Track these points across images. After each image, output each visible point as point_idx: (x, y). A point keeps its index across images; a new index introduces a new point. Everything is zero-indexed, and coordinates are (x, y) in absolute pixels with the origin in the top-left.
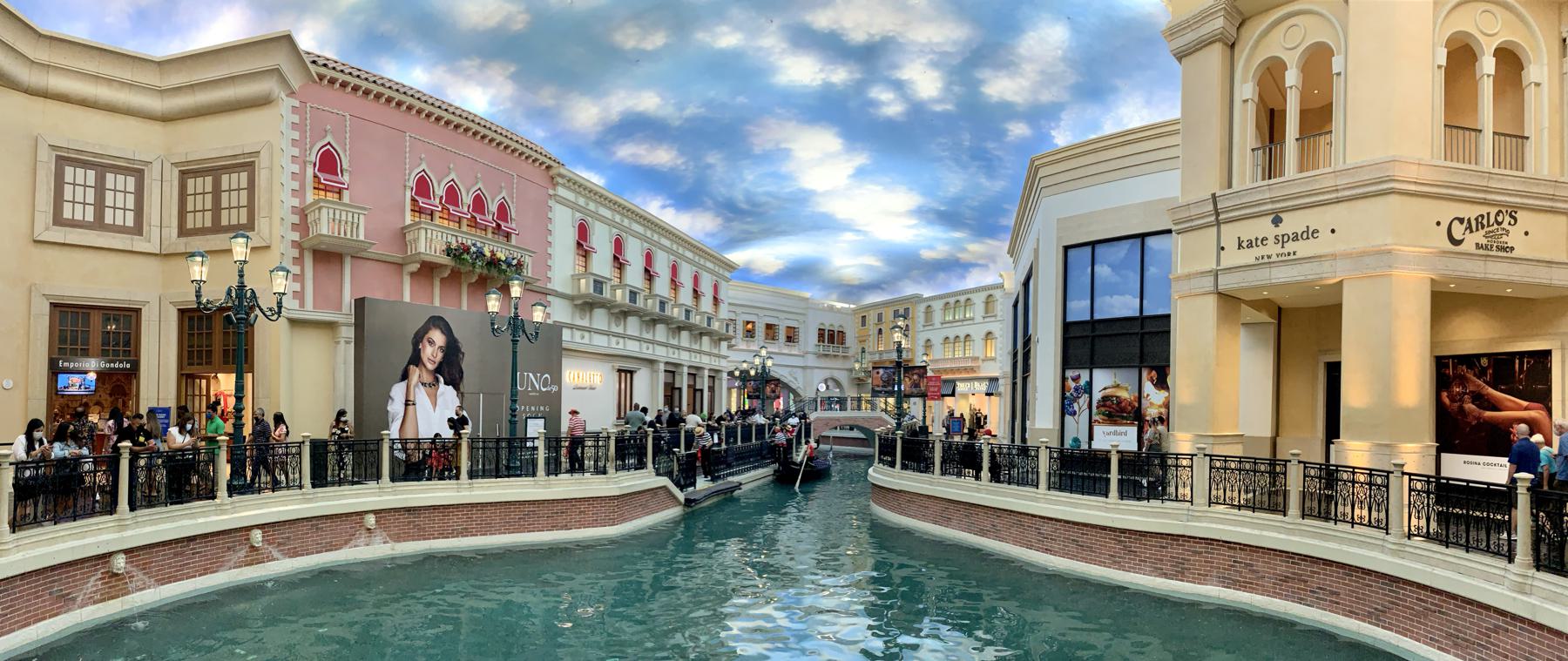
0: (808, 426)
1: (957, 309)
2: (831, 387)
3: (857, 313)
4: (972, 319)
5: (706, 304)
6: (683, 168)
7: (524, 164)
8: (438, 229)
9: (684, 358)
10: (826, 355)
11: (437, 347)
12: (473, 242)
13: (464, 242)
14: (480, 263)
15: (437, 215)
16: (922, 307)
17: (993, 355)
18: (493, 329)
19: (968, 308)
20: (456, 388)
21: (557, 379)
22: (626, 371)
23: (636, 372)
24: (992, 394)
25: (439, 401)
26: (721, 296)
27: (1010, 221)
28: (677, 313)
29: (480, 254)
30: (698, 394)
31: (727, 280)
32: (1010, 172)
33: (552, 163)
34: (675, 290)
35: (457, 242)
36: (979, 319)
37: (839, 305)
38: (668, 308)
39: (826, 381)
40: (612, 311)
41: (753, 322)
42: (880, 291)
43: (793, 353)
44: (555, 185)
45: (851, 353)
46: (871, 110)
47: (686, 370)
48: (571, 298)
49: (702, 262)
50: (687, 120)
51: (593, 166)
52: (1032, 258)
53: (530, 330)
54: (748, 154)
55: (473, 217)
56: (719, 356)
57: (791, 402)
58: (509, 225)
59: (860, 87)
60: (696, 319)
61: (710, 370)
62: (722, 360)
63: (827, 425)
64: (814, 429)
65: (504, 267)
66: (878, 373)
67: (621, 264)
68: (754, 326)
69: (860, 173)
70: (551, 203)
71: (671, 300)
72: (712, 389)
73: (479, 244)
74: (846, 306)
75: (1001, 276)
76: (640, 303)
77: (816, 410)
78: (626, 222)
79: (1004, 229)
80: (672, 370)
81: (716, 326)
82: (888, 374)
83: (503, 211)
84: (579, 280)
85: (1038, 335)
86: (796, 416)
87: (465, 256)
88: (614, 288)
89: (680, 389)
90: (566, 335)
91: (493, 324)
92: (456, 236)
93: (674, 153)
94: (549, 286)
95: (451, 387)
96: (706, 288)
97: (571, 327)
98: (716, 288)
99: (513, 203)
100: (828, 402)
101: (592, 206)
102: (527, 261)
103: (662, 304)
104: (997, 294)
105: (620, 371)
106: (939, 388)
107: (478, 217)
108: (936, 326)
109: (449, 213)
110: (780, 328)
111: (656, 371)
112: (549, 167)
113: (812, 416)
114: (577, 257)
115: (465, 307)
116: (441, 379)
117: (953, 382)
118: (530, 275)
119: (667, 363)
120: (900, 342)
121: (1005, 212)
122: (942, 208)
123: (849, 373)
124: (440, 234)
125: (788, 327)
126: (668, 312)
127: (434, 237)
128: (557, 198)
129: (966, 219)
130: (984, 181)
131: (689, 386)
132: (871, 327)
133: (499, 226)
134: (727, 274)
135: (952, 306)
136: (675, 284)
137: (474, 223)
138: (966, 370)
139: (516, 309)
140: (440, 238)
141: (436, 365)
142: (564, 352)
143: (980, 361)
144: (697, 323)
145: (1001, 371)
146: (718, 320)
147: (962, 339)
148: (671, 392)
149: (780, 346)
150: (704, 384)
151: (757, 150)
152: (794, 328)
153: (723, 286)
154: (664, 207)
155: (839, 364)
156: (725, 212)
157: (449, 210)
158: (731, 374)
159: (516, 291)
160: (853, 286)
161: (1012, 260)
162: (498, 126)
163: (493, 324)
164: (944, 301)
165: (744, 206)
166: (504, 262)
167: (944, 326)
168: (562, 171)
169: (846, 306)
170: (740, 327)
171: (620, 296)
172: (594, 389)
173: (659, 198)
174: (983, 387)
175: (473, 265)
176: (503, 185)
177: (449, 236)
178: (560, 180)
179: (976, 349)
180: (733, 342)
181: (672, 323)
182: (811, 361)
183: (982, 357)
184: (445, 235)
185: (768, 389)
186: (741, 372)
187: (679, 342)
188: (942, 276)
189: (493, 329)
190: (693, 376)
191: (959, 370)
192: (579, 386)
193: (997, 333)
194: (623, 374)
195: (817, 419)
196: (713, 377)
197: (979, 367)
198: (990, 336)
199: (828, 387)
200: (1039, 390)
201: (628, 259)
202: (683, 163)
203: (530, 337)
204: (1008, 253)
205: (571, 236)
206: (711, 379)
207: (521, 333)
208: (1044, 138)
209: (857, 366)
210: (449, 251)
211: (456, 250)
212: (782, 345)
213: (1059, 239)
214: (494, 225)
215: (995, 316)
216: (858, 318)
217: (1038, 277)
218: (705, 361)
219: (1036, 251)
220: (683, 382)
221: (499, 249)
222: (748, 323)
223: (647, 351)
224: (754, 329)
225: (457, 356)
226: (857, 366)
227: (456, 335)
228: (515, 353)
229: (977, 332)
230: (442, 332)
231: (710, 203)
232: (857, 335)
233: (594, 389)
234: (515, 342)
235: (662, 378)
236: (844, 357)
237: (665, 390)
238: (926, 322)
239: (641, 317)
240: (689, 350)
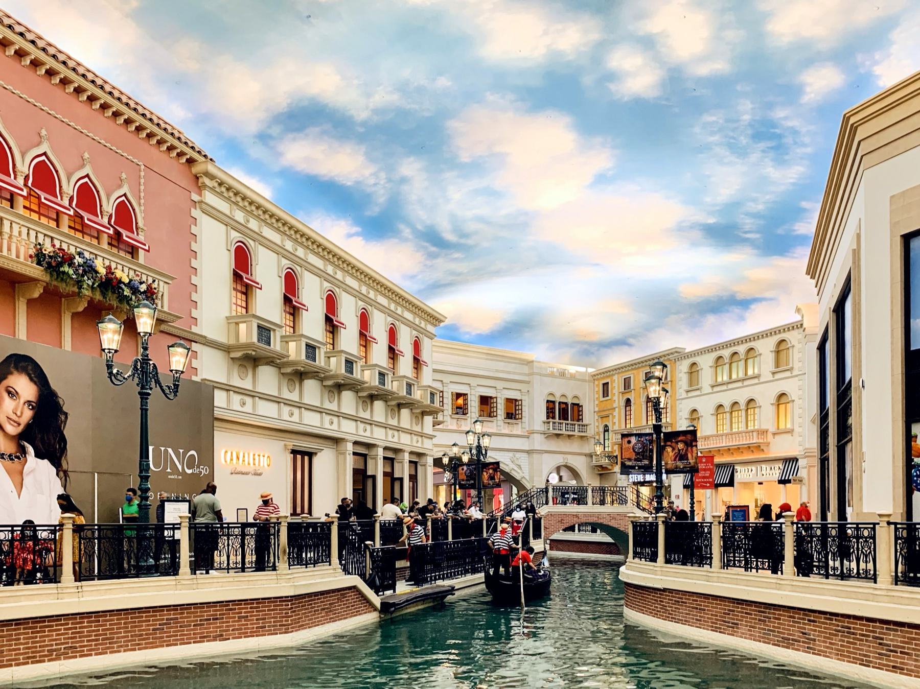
0: (537, 523)
1: (734, 365)
2: (564, 479)
3: (598, 379)
4: (757, 377)
5: (405, 366)
6: (372, 181)
7: (154, 152)
8: (22, 223)
9: (379, 436)
10: (558, 435)
11: (22, 401)
12: (78, 250)
13: (65, 247)
14: (90, 283)
15: (20, 202)
16: (684, 366)
17: (789, 426)
18: (111, 373)
19: (750, 362)
20: (56, 462)
21: (208, 457)
22: (303, 453)
23: (316, 454)
24: (789, 481)
25: (27, 480)
26: (425, 356)
27: (808, 227)
28: (369, 378)
29: (89, 269)
30: (397, 486)
31: (431, 337)
32: (809, 150)
33: (196, 156)
34: (365, 347)
35: (54, 246)
36: (766, 375)
37: (573, 369)
38: (357, 369)
39: (558, 469)
40: (283, 371)
41: (465, 395)
42: (625, 348)
43: (515, 432)
44: (200, 188)
45: (591, 431)
46: (612, 87)
47: (380, 453)
48: (226, 349)
49: (399, 311)
50: (376, 111)
51: (255, 168)
52: (850, 264)
53: (167, 382)
54: (453, 164)
55: (77, 215)
56: (422, 435)
57: (514, 496)
58: (135, 236)
59: (600, 50)
60: (392, 385)
61: (411, 453)
62: (426, 440)
63: (561, 521)
64: (545, 527)
65: (127, 292)
66: (629, 442)
67: (294, 307)
68: (465, 400)
69: (601, 179)
70: (196, 213)
71: (360, 359)
72: (413, 478)
73: (87, 255)
74: (583, 369)
75: (798, 310)
76: (321, 361)
77: (547, 503)
78: (300, 252)
79: (800, 240)
80: (363, 451)
81: (417, 394)
82: (643, 443)
83: (124, 214)
84: (237, 324)
85: (864, 377)
86: (521, 509)
87: (66, 268)
88: (285, 340)
89: (374, 478)
90: (220, 398)
91: (109, 367)
92: (52, 238)
93: (361, 159)
94: (194, 329)
95: (46, 461)
96: (405, 345)
97: (227, 388)
98: (417, 346)
99: (140, 205)
100: (563, 496)
101: (253, 224)
102: (161, 289)
103: (349, 364)
104: (793, 337)
105: (294, 452)
106: (712, 474)
107: (86, 215)
108: (705, 391)
109: (40, 204)
110: (499, 400)
111: (341, 454)
112: (191, 161)
113: (542, 511)
114: (234, 293)
115: (67, 344)
116: (30, 449)
117: (730, 468)
118: (166, 309)
119: (356, 443)
120: (658, 398)
121: (799, 213)
122: (711, 221)
123: (589, 459)
124: (25, 231)
125: (507, 399)
126: (357, 374)
127: (15, 233)
128: (204, 206)
129: (746, 232)
130: (771, 171)
131: (385, 474)
132: (616, 398)
133: (118, 234)
134: (430, 328)
135: (727, 361)
136: (365, 338)
137: (80, 226)
138: (749, 448)
139: (145, 349)
140: (24, 236)
141: (21, 427)
142: (216, 424)
143: (770, 436)
144: (395, 389)
145: (801, 448)
146: (420, 388)
147: (743, 406)
148: (361, 477)
149: (498, 424)
150: (403, 470)
151: (465, 158)
152: (516, 400)
153: (426, 344)
154: (350, 236)
155: (574, 446)
156: (426, 244)
157: (39, 198)
158: (438, 462)
159: (145, 323)
160: (591, 344)
161: (814, 282)
162: (114, 88)
163: (109, 367)
164: (715, 355)
165: (450, 237)
166: (127, 285)
167: (716, 389)
168: (211, 168)
169: (583, 369)
170: (448, 400)
171: (295, 352)
172: (260, 474)
173: (343, 223)
174: (775, 472)
175: (79, 284)
176: (124, 176)
177: (41, 237)
178: (207, 181)
179: (765, 418)
180: (440, 417)
181: (362, 390)
182: (538, 442)
183: (772, 429)
184: (33, 234)
185: (485, 476)
186: (451, 459)
187: (372, 416)
188: (711, 319)
189: (111, 373)
190: (389, 461)
191: (738, 449)
192: (239, 469)
193: (793, 393)
194: (299, 457)
195: (550, 515)
196: (416, 463)
197: (768, 444)
198: (783, 400)
199: (561, 478)
200: (866, 458)
201: (304, 302)
202: (371, 175)
203: (167, 391)
204: (808, 273)
205: (226, 263)
206: (413, 465)
207: (153, 384)
208: (861, 80)
209: (599, 449)
210: (39, 257)
211: (50, 257)
212: (501, 423)
213: (894, 225)
214: (111, 232)
215: (791, 370)
216: (598, 386)
217: (860, 296)
218: (405, 441)
219: (856, 254)
220: (377, 468)
221: (120, 267)
222: (458, 395)
223: (330, 426)
224: (465, 404)
225: (57, 418)
226: (599, 449)
227: (54, 384)
228: (144, 412)
229: (765, 394)
230: (31, 379)
231: (407, 232)
232: (597, 409)
233: (260, 474)
234: (144, 396)
235: (350, 463)
236: (582, 437)
237: (355, 482)
238: (691, 385)
239: (322, 380)
240: (385, 427)
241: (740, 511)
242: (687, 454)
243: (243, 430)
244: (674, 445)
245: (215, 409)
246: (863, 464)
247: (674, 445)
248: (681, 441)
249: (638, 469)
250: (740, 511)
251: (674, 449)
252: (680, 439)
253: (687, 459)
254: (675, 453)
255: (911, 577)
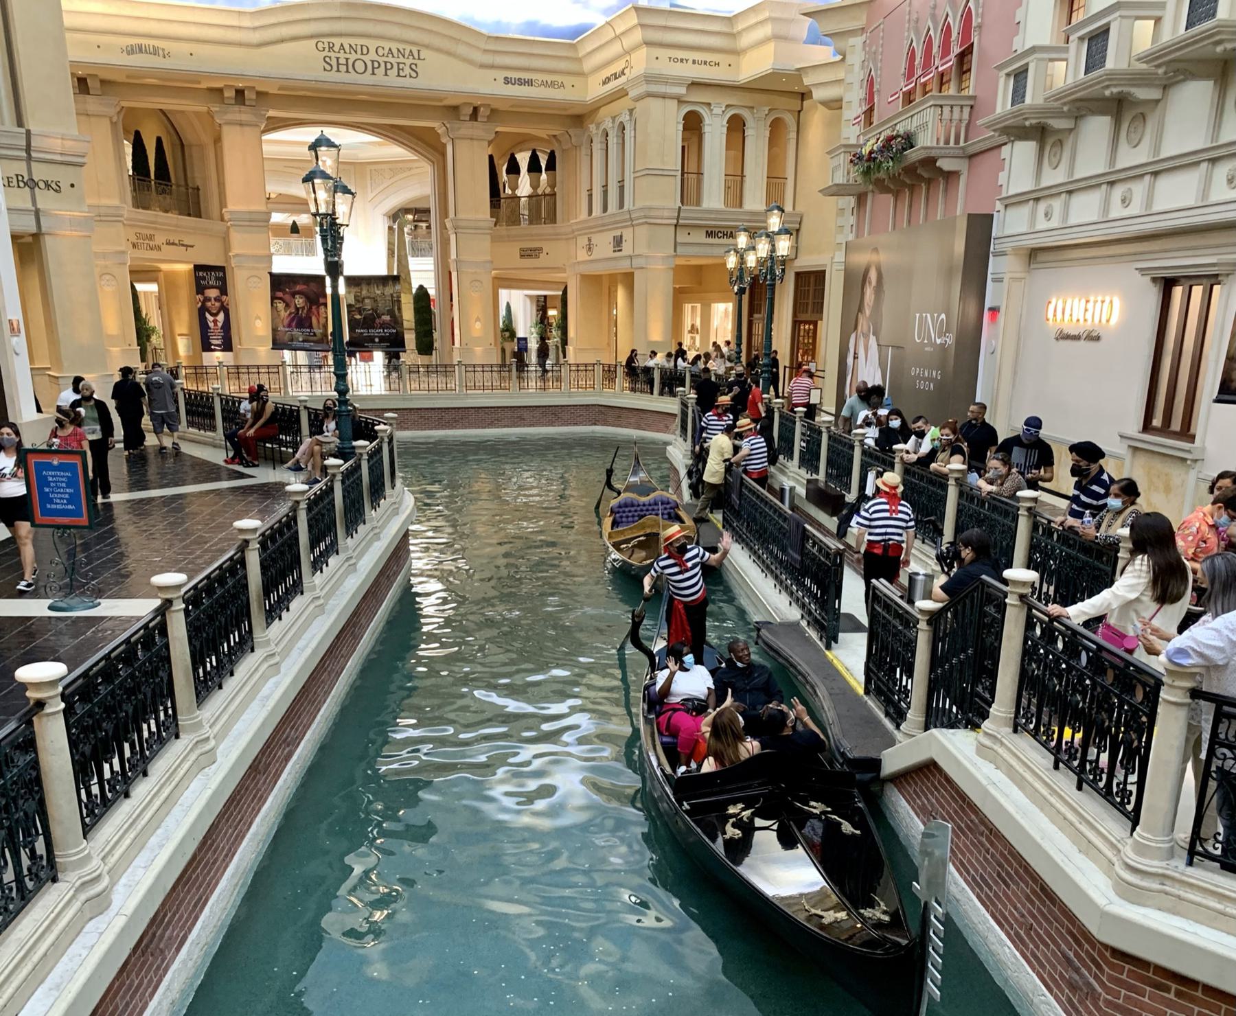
172: (1098, 338)
233: (1098, 338)
241: (61, 467)
242: (311, 318)
243: (386, 18)
244: (287, 297)
245: (68, 35)
246: (698, 323)
247: (287, 297)
248: (299, 293)
249: (380, 342)
250: (61, 467)
251: (287, 306)
252: (298, 288)
253: (311, 327)
254: (290, 314)
255: (754, 759)
